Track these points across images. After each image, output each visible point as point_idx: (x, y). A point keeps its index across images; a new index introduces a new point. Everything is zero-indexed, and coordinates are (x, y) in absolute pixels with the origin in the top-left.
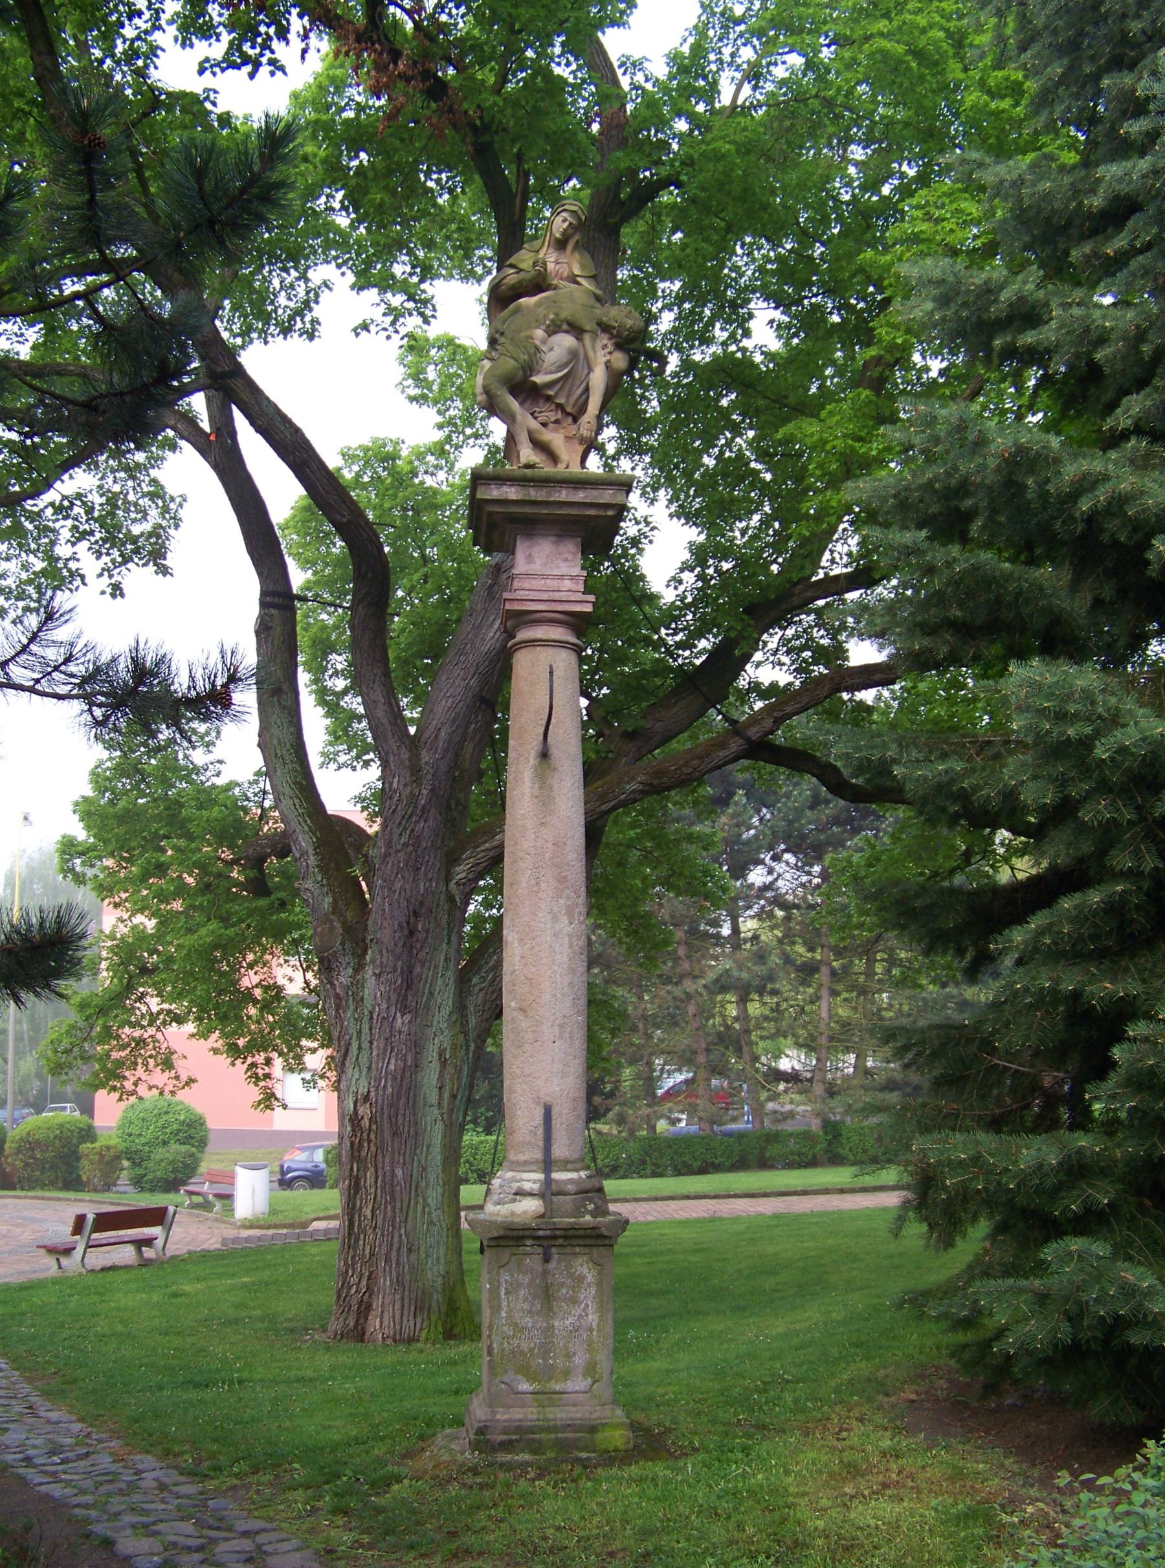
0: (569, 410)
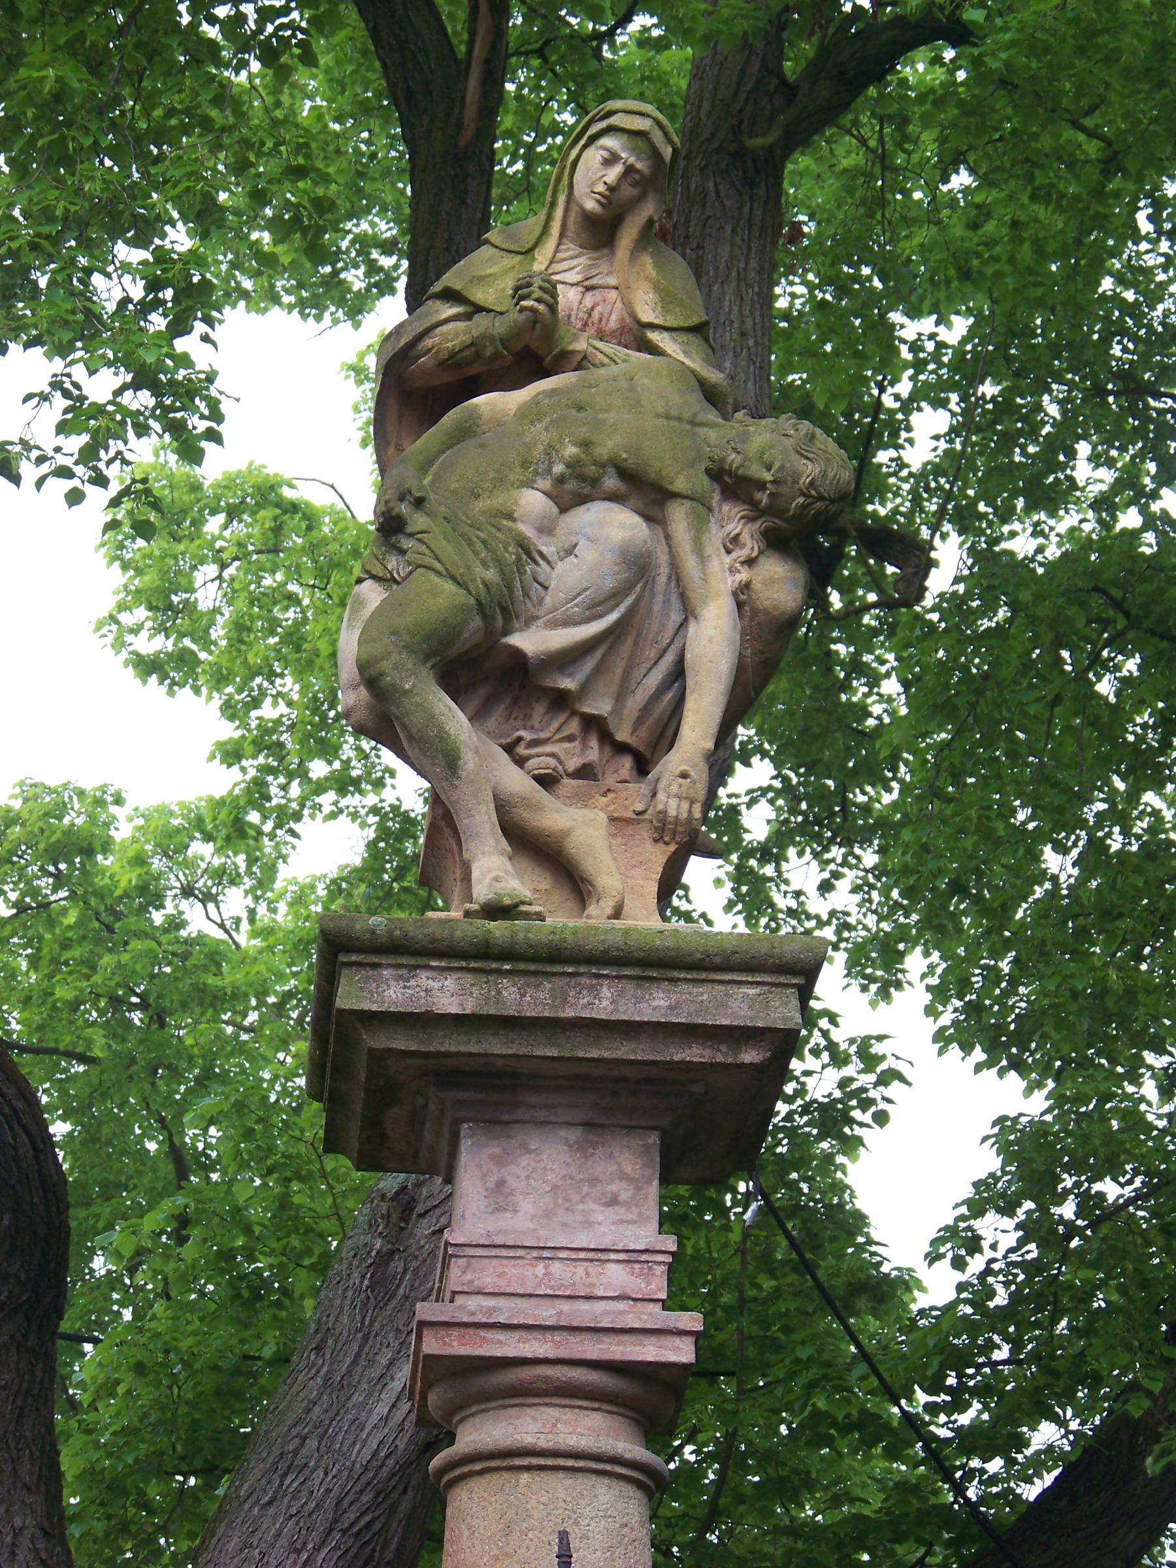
0: (623, 735)
